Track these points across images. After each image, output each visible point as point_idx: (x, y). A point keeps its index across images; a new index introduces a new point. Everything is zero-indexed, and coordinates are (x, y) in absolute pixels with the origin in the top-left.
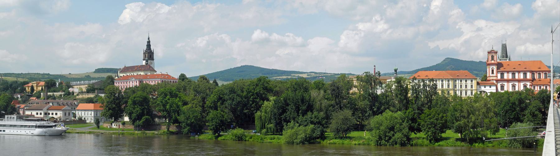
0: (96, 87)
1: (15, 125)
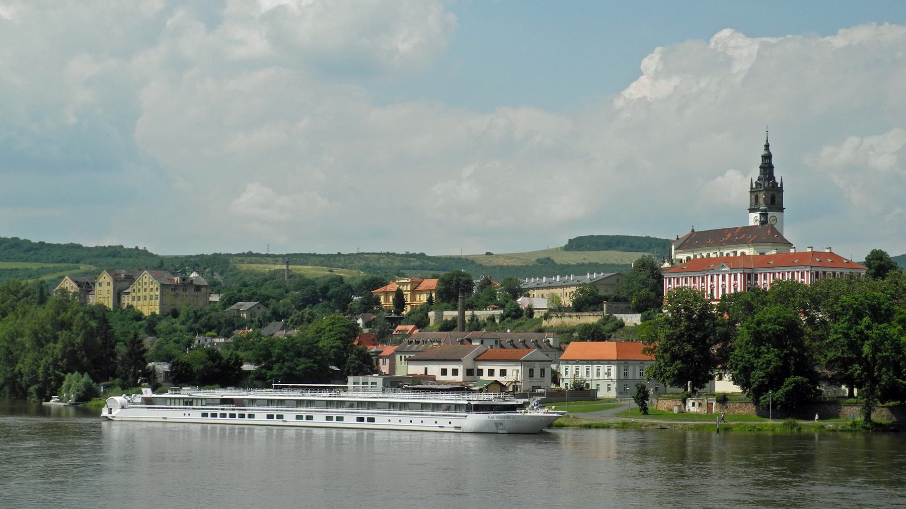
0: (602, 293)
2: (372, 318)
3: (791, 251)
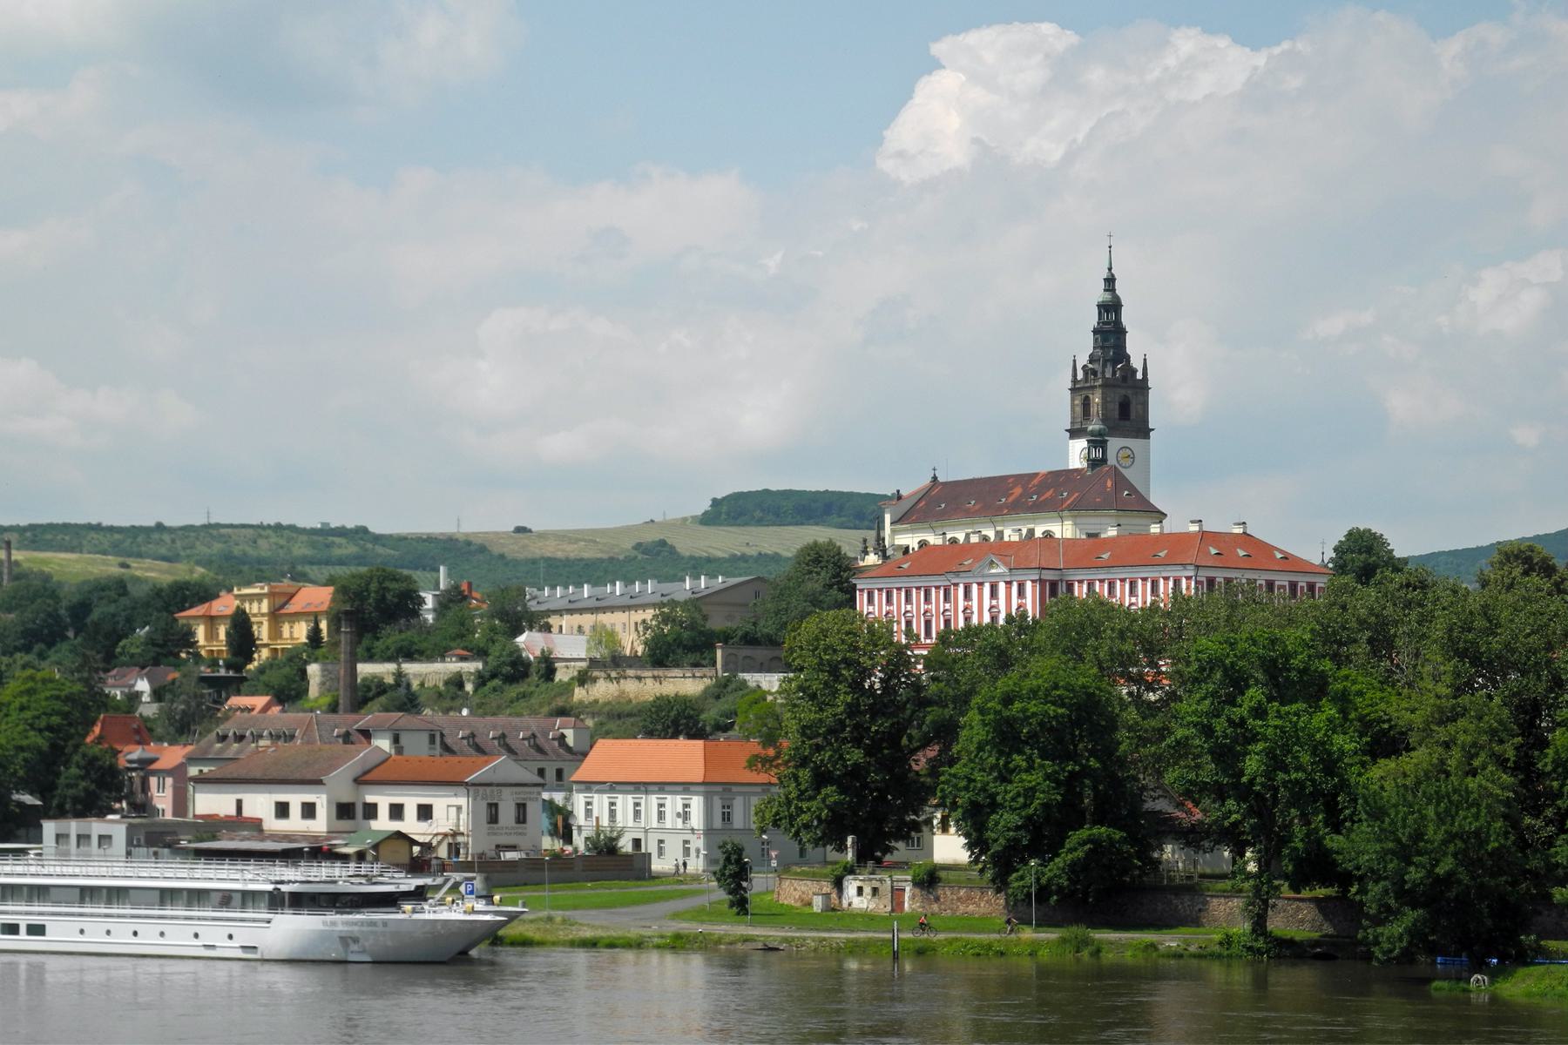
0: (717, 623)
2: (170, 677)
3: (1152, 531)
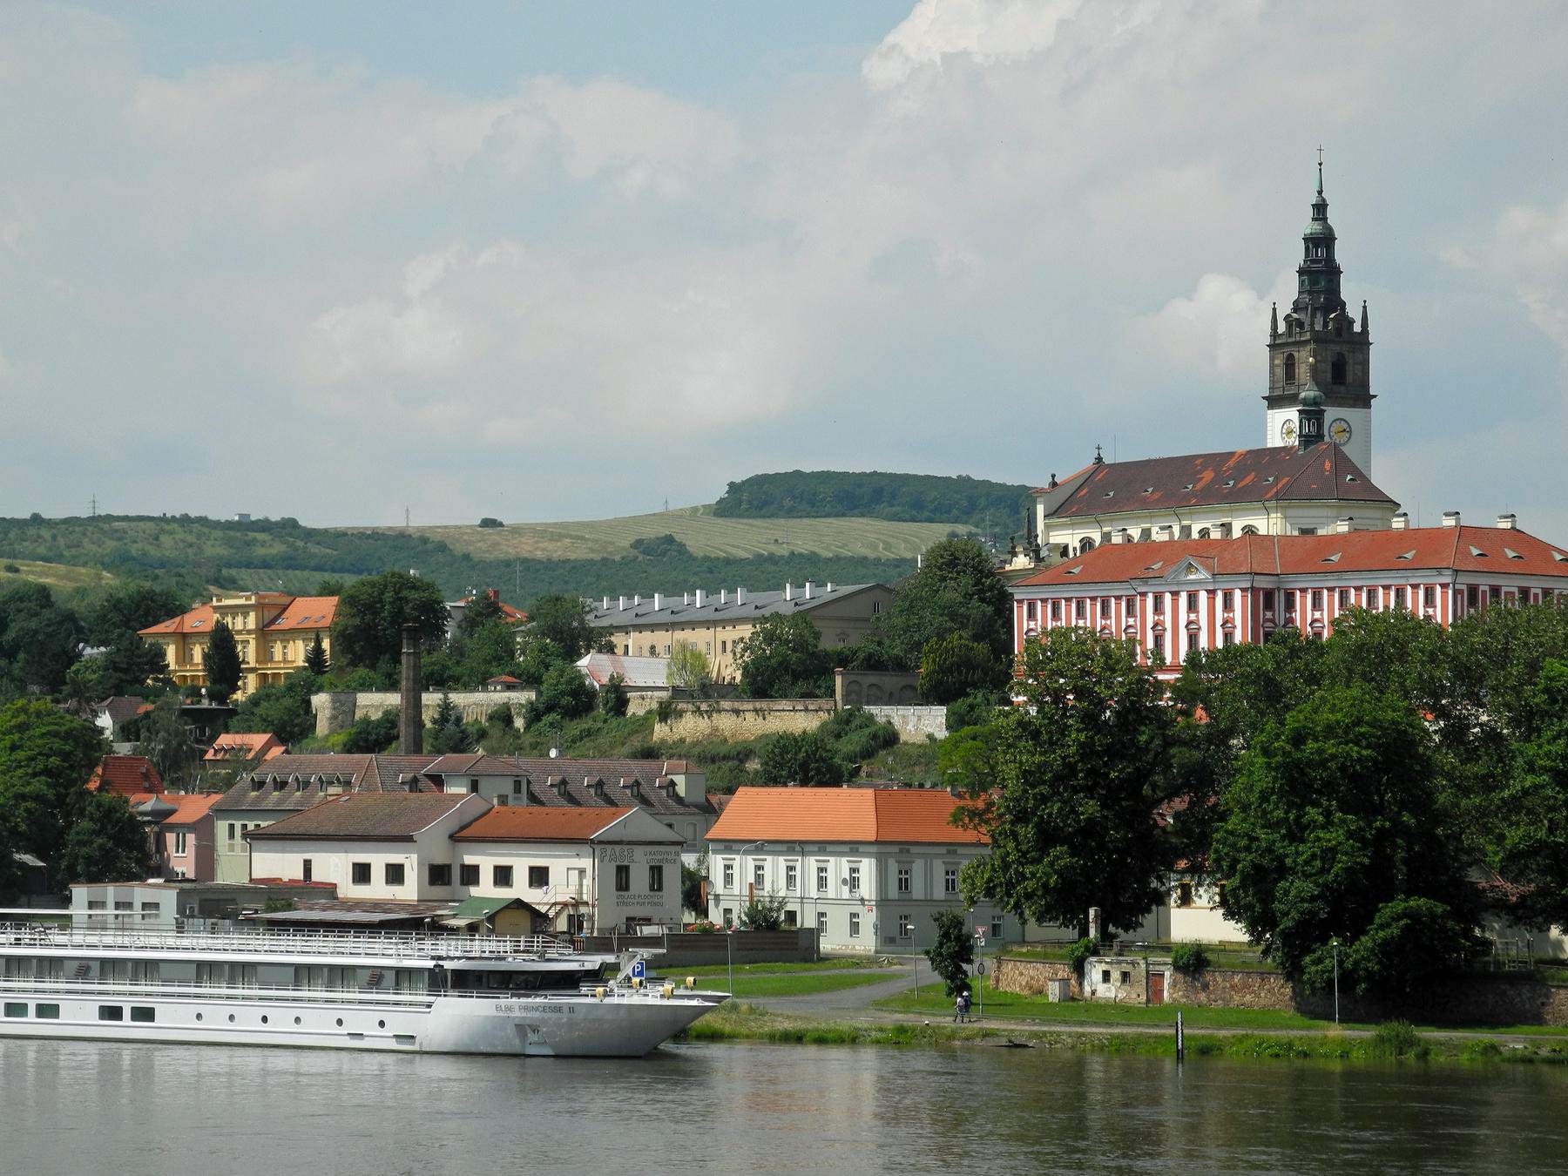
0: (829, 643)
1: (245, 966)
3: (1394, 525)
